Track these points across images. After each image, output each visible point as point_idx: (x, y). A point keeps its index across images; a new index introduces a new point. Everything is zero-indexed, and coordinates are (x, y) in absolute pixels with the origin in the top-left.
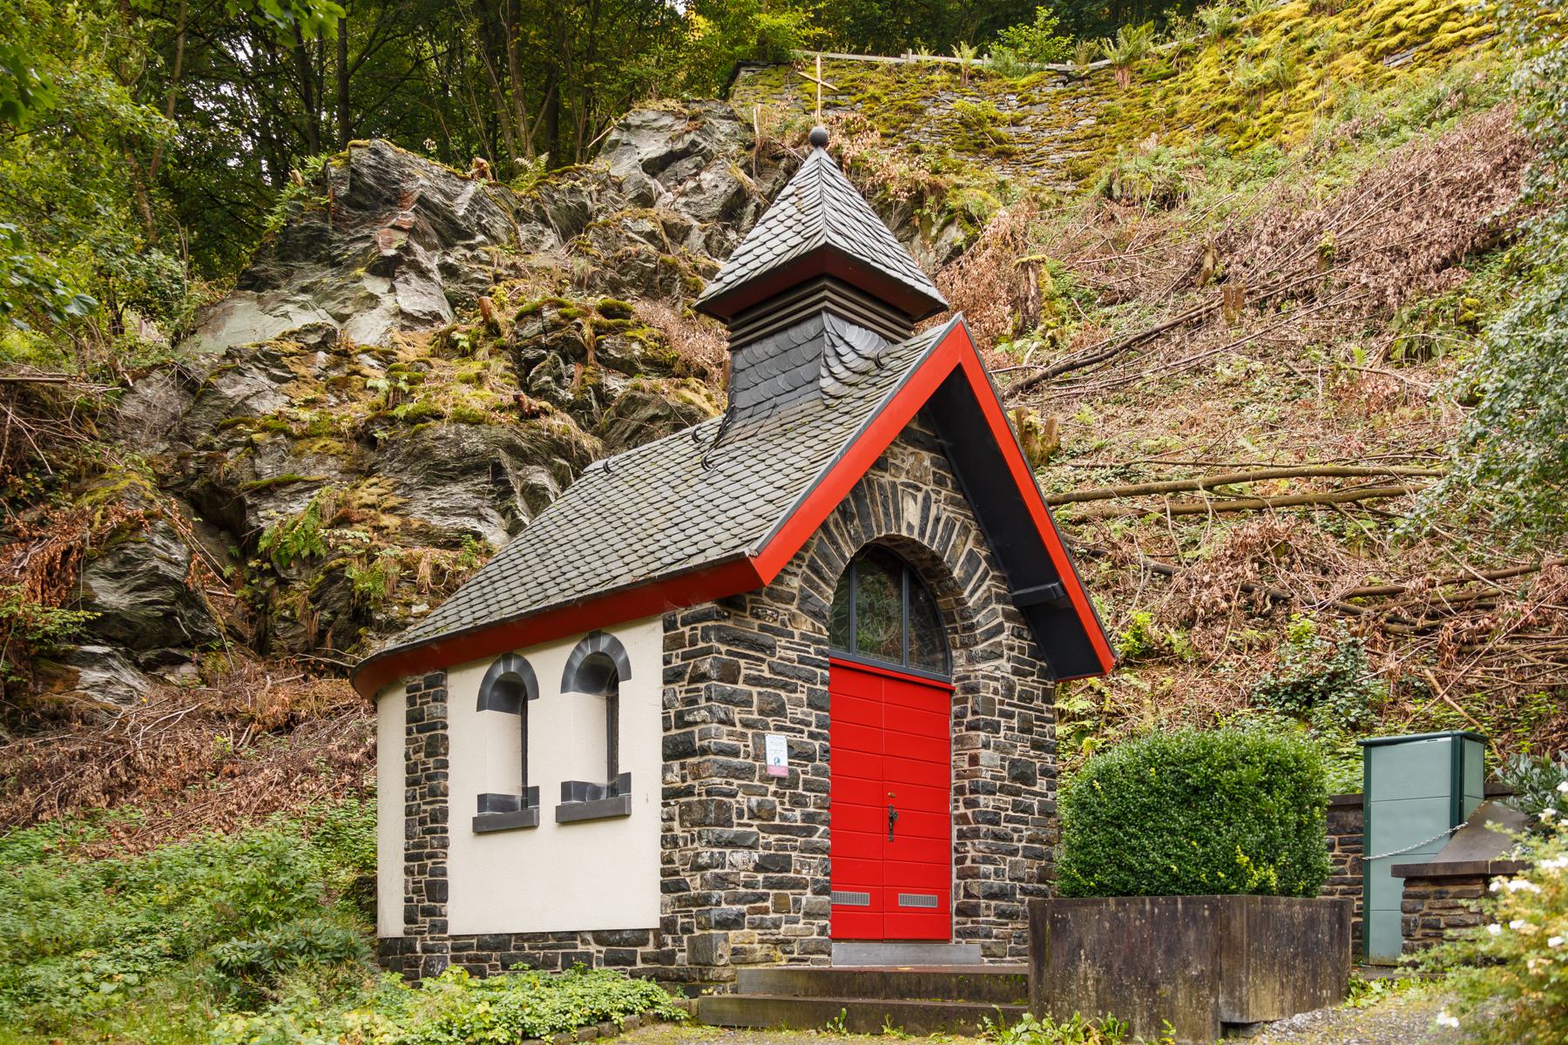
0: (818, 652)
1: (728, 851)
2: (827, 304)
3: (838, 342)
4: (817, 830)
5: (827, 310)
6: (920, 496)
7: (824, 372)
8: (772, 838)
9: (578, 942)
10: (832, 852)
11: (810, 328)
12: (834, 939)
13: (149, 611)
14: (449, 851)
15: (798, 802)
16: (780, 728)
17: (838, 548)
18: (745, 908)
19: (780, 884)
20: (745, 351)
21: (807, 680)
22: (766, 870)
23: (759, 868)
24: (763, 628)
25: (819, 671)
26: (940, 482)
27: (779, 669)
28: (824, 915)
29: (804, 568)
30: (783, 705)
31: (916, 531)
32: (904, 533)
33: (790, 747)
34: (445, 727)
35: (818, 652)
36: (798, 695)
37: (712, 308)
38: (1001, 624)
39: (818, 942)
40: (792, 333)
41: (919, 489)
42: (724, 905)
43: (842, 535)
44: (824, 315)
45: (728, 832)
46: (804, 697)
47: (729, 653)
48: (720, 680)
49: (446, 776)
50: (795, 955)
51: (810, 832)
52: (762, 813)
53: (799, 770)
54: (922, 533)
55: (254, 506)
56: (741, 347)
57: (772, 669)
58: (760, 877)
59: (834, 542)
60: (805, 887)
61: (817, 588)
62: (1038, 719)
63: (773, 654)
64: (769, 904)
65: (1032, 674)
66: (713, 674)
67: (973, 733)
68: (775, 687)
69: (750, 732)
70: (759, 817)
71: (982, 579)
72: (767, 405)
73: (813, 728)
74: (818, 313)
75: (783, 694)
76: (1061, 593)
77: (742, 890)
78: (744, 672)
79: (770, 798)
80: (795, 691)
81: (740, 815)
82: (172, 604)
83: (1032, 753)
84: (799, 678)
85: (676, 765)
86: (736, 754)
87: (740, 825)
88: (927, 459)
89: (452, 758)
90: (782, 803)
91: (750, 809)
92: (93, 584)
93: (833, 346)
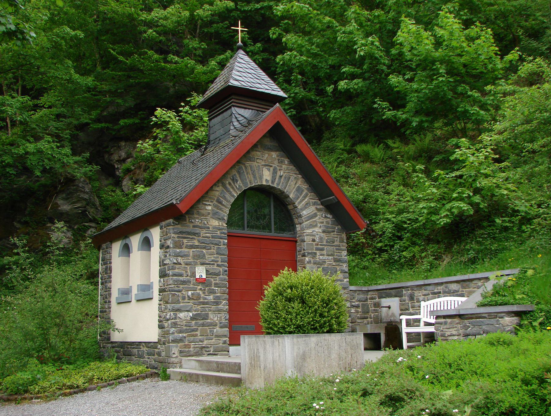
0: (221, 233)
1: (177, 313)
2: (233, 104)
3: (237, 116)
4: (221, 302)
5: (234, 106)
6: (272, 169)
7: (232, 128)
8: (199, 307)
9: (141, 347)
10: (230, 311)
11: (229, 112)
12: (231, 344)
13: (76, 211)
14: (112, 309)
15: (212, 292)
16: (202, 264)
17: (230, 193)
18: (185, 335)
19: (203, 325)
20: (213, 120)
21: (216, 244)
22: (197, 319)
23: (192, 319)
24: (194, 226)
25: (222, 240)
26: (281, 162)
27: (203, 241)
28: (225, 336)
29: (215, 202)
30: (204, 255)
31: (270, 182)
32: (264, 183)
33: (207, 271)
34: (111, 263)
35: (221, 233)
36: (212, 250)
37: (202, 106)
38: (315, 213)
39: (223, 347)
40: (225, 114)
41: (271, 166)
42: (176, 334)
43: (233, 188)
44: (233, 108)
45: (177, 306)
46: (215, 251)
47: (178, 237)
48: (174, 248)
49: (110, 282)
50: (211, 352)
51: (217, 304)
52: (195, 298)
53: (212, 280)
54: (273, 182)
55: (118, 168)
56: (214, 118)
57: (199, 241)
58: (194, 322)
59: (228, 191)
60: (216, 325)
61: (221, 209)
62: (337, 249)
63: (199, 236)
64: (198, 333)
65: (334, 231)
66: (171, 246)
67: (303, 258)
68: (201, 248)
69: (188, 267)
70: (193, 299)
71: (305, 197)
72: (218, 139)
73: (220, 263)
74: (230, 108)
75: (204, 251)
76: (337, 200)
77: (185, 328)
78: (185, 244)
79: (198, 291)
80: (210, 249)
81: (184, 298)
82: (85, 207)
83: (334, 264)
84: (212, 244)
85: (162, 280)
86: (181, 275)
87: (183, 303)
88: (274, 155)
89: (113, 274)
90: (204, 293)
91: (188, 296)
92: (59, 202)
93: (236, 118)
